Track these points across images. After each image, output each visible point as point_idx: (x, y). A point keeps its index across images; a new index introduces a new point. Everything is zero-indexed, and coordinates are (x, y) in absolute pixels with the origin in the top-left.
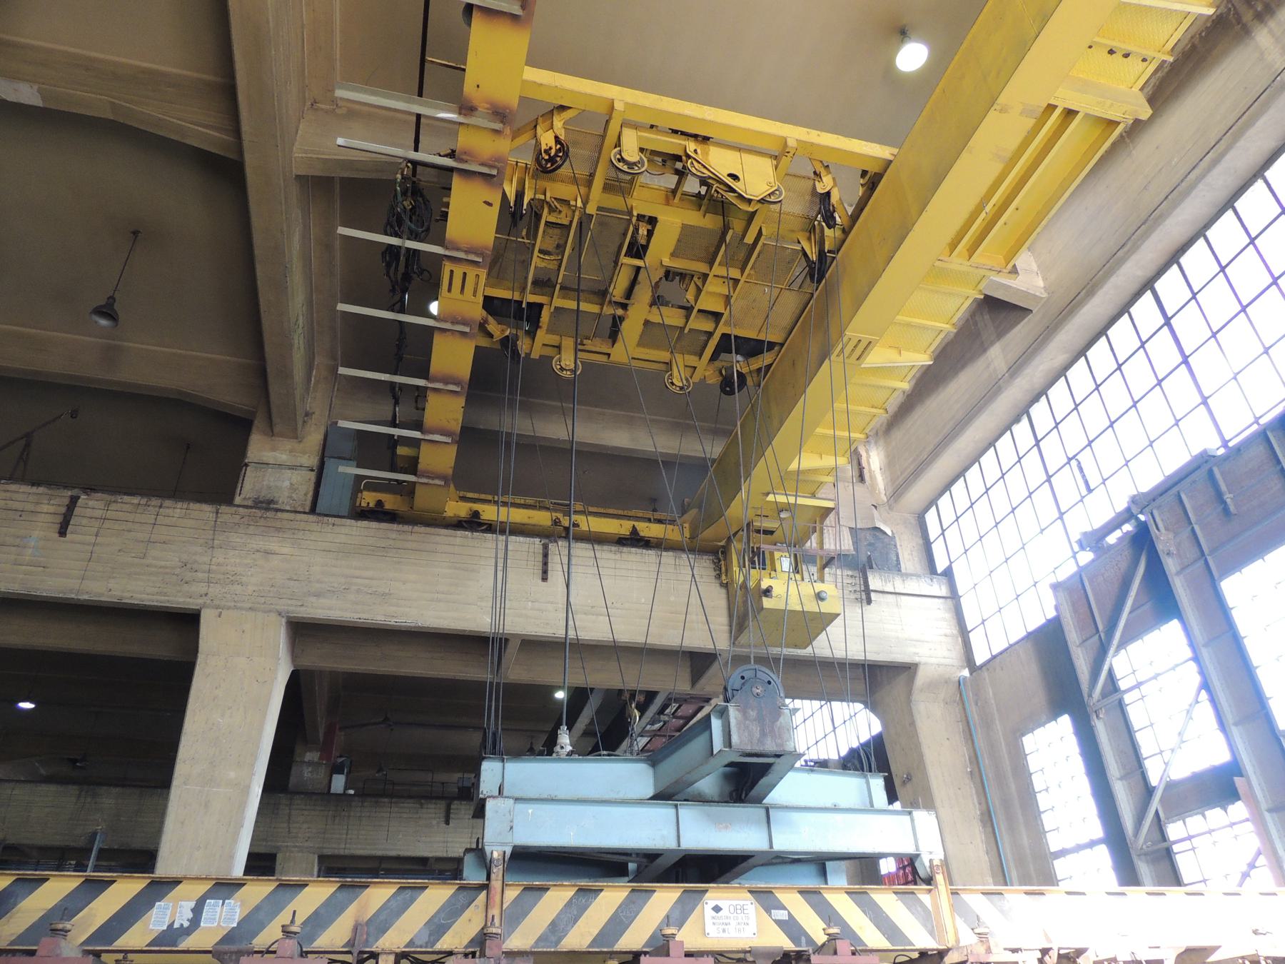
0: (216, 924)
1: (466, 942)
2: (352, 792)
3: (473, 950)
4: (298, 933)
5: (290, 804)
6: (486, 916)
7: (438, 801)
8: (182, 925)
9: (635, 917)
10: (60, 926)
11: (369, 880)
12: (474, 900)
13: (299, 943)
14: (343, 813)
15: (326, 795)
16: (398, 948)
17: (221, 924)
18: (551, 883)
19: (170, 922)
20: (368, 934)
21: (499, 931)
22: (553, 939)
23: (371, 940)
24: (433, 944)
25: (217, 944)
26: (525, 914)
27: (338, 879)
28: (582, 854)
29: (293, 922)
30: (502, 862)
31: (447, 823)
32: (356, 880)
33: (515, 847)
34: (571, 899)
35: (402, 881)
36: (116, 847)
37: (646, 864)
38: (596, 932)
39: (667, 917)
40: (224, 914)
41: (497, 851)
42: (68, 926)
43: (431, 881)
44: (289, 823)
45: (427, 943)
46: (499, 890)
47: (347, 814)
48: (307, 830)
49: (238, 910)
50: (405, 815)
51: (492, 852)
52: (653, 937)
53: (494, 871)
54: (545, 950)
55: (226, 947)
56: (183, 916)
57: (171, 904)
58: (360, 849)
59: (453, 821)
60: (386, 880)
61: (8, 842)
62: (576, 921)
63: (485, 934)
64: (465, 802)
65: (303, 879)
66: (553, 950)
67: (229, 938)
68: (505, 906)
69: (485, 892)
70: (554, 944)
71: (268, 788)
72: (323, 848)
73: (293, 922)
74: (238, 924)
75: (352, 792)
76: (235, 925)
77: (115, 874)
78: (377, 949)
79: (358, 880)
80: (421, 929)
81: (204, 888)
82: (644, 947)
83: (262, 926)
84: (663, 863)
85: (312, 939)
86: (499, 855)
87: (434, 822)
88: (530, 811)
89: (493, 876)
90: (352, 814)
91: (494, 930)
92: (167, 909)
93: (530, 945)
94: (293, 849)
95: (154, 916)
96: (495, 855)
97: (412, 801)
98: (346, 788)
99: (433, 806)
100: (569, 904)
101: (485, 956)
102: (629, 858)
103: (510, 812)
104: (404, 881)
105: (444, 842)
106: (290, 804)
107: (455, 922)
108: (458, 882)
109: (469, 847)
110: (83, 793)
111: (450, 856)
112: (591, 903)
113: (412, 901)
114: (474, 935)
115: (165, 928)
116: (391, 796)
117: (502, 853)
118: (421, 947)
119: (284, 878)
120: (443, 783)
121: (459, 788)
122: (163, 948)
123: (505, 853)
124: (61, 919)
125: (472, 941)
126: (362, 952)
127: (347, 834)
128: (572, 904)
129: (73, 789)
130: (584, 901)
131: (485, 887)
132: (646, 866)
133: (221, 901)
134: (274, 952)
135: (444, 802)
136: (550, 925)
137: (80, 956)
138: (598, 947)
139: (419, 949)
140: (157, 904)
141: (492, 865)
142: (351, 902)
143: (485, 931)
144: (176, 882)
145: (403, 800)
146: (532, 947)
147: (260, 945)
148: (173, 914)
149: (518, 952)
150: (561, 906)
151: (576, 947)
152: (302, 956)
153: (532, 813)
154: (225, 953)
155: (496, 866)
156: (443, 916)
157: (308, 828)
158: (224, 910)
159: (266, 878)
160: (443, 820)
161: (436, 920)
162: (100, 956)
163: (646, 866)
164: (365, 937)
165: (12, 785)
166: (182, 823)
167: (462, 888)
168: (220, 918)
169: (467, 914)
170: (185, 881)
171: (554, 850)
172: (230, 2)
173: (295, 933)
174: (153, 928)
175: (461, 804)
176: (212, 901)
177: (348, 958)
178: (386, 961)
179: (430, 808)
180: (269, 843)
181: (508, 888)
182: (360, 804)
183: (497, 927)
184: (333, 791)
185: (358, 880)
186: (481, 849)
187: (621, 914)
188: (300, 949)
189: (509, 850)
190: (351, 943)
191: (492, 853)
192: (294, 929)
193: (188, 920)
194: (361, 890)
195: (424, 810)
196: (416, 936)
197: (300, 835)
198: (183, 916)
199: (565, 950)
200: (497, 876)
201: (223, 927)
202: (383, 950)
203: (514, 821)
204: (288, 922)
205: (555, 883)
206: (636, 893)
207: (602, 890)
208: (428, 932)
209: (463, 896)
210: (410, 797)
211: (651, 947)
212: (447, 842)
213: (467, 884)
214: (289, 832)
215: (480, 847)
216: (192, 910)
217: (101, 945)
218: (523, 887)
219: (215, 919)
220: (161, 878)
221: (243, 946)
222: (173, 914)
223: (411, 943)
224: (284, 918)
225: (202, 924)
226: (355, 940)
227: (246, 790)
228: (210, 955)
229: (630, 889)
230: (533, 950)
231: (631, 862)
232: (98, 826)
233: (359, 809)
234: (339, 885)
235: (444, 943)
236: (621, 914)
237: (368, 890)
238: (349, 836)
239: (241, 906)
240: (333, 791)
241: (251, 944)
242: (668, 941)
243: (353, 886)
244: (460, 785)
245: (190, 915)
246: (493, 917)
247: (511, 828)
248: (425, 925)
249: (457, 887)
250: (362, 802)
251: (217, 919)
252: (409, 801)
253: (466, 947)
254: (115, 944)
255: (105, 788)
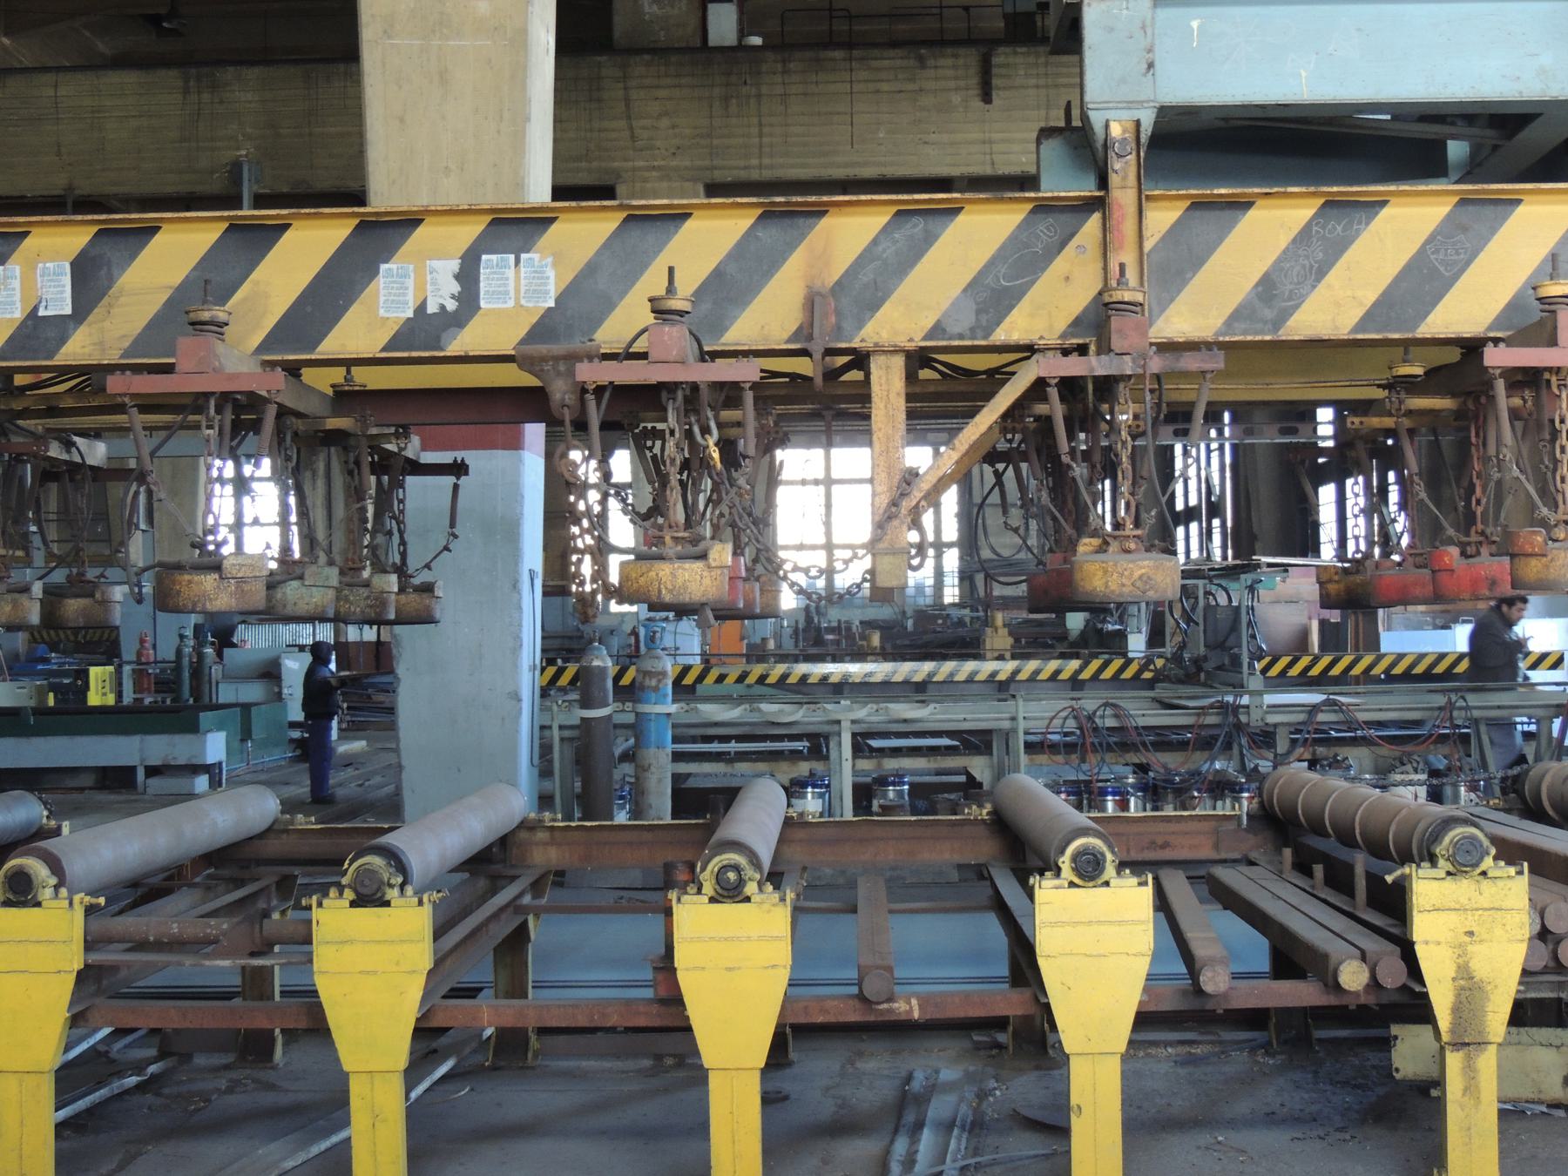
0: (511, 304)
1: (1062, 324)
2: (756, 41)
3: (1080, 341)
4: (687, 312)
5: (625, 77)
6: (1105, 269)
7: (962, 51)
8: (443, 307)
9: (1468, 263)
10: (206, 316)
11: (825, 198)
12: (1072, 235)
13: (691, 333)
14: (745, 90)
15: (700, 50)
16: (911, 340)
17: (523, 302)
18: (1257, 190)
19: (419, 303)
20: (838, 313)
21: (1139, 297)
22: (1269, 314)
23: (847, 325)
24: (988, 332)
25: (523, 342)
26: (1197, 262)
27: (754, 200)
28: (1330, 121)
29: (671, 289)
30: (1134, 145)
31: (987, 97)
32: (794, 199)
33: (1163, 111)
34: (1308, 225)
35: (900, 197)
36: (285, 190)
37: (1494, 142)
38: (1370, 296)
39: (1554, 257)
40: (523, 282)
41: (1119, 121)
42: (222, 316)
43: (968, 195)
44: (629, 118)
45: (972, 329)
46: (1131, 209)
47: (754, 91)
48: (671, 131)
49: (551, 273)
50: (885, 87)
51: (1107, 122)
52: (1514, 306)
53: (1117, 166)
54: (1249, 338)
55: (542, 349)
56: (443, 293)
57: (411, 267)
58: (793, 166)
59: (1001, 93)
60: (863, 197)
61: (78, 192)
62: (1321, 273)
63: (1106, 305)
64: (1024, 50)
65: (676, 202)
66: (1268, 338)
67: (544, 328)
68: (1148, 245)
69: (1096, 217)
70: (1270, 326)
71: (570, 44)
72: (715, 168)
73: (671, 289)
74: (557, 301)
75: (756, 41)
76: (552, 304)
77: (284, 212)
78: (864, 345)
79: (799, 199)
80: (957, 299)
81: (470, 230)
82: (1490, 328)
83: (607, 305)
84: (1536, 138)
85: (720, 328)
86: (1124, 131)
87: (956, 99)
88: (1195, 24)
89: (1114, 180)
90: (764, 90)
91: (1127, 296)
92: (406, 276)
93: (1214, 330)
94: (647, 174)
95: (382, 292)
96: (1116, 130)
97: (899, 52)
98: (742, 33)
99: (949, 62)
100: (1304, 236)
101: (1111, 350)
102: (1445, 129)
103: (1143, 28)
104: (905, 197)
105: (984, 142)
106: (625, 77)
107: (1033, 282)
108: (1032, 195)
109: (1043, 124)
110: (192, 83)
111: (1000, 172)
112: (1358, 234)
113: (929, 240)
114: (1081, 309)
115: (410, 314)
116: (849, 45)
117: (1131, 126)
118: (961, 337)
119: (635, 203)
120: (966, 9)
121: (1005, 16)
122: (415, 354)
123: (1138, 123)
124: (205, 302)
125: (1077, 323)
126: (831, 352)
127: (761, 136)
128: (1310, 237)
129: (171, 77)
130: (1339, 229)
131: (1097, 204)
132: (1495, 148)
133: (512, 257)
134: (643, 356)
135: (973, 51)
136: (1257, 285)
137: (259, 370)
138: (1378, 331)
139: (956, 343)
140: (383, 267)
141: (1111, 154)
142: (791, 247)
143: (1107, 299)
144: (410, 222)
145: (876, 52)
146: (1217, 334)
147: (612, 342)
148: (420, 286)
149: (1185, 343)
150: (1284, 240)
151: (1324, 332)
152: (703, 360)
153: (1199, 27)
154: (544, 359)
155: (1120, 156)
156: (1003, 270)
157: (674, 127)
158: (522, 275)
159: (598, 203)
160: (976, 92)
161: (989, 280)
162: (300, 375)
163: (1495, 148)
164: (833, 319)
165: (49, 78)
166: (402, 120)
167: (1043, 208)
168: (517, 291)
169: (1060, 264)
170: (428, 220)
171: (1260, 114)
172: (617, 4)
173: (681, 313)
174: (387, 315)
175: (1016, 53)
176: (494, 257)
177: (802, 366)
178: (888, 367)
179: (942, 67)
180: (595, 164)
181: (1152, 205)
182: (779, 67)
183: (1134, 289)
184: (714, 40)
185: (799, 199)
186: (1082, 129)
187: (1432, 257)
188: (695, 345)
189: (1148, 119)
190: (804, 332)
191: (1107, 126)
192: (676, 304)
193: (453, 297)
194: (810, 221)
195: (931, 73)
196: (946, 314)
197: (658, 143)
198: (443, 293)
199: (1296, 338)
200: (1125, 178)
201: (527, 309)
202: (876, 345)
203: (1157, 49)
204: (660, 291)
205: (1268, 190)
206: (1471, 208)
207: (1384, 203)
208: (974, 307)
209: (1046, 227)
210: (894, 44)
211: (1508, 329)
212: (991, 142)
213: (1053, 198)
214: (633, 137)
215: (1076, 123)
216: (457, 277)
217: (295, 352)
218: (1189, 203)
219: (507, 293)
220: (377, 214)
221: (576, 345)
222: (420, 286)
223: (937, 330)
224: (652, 282)
225: (482, 304)
226: (812, 325)
227: (520, 40)
228: (514, 366)
229: (1456, 199)
230: (1221, 339)
231: (1454, 137)
232: (238, 149)
233: (778, 78)
234: (759, 211)
235: (1015, 327)
236: (1432, 257)
237: (825, 222)
238: (765, 140)
239: (554, 265)
240: (714, 40)
241: (591, 340)
242: (1554, 312)
243: (790, 214)
244: (1009, 9)
245: (455, 288)
246: (1122, 266)
247: (1151, 66)
248: (965, 290)
249: (1030, 206)
250: (784, 61)
251: (512, 294)
252: (891, 53)
253: (1063, 336)
254: (320, 348)
255: (231, 69)
